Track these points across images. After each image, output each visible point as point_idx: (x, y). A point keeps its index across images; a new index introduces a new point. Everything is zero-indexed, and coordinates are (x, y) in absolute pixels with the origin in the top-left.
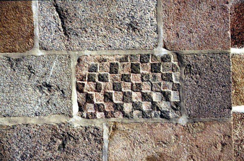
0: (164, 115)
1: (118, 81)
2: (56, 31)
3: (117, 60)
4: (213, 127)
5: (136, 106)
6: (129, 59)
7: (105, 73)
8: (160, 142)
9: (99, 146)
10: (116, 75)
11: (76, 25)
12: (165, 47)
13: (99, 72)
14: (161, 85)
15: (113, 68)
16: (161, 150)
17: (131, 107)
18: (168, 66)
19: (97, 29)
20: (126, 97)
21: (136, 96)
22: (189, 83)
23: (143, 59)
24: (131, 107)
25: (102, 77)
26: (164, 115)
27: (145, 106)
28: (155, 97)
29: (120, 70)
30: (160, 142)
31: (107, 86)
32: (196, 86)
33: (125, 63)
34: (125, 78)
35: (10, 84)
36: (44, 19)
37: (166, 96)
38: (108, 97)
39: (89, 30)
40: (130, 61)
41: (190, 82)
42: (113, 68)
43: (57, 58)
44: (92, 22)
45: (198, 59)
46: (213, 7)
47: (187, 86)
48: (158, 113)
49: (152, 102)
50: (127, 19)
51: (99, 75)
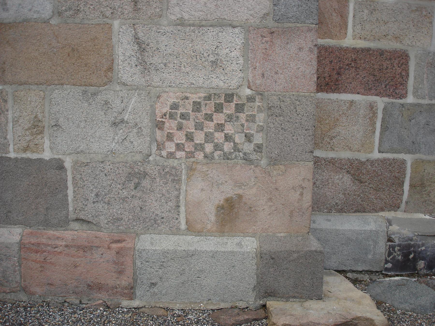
0: (247, 159)
1: (199, 120)
2: (136, 65)
3: (200, 98)
4: (294, 170)
5: (217, 147)
6: (213, 97)
7: (186, 111)
8: (239, 184)
9: (177, 186)
10: (198, 114)
11: (156, 60)
12: (249, 87)
13: (181, 110)
14: (244, 126)
15: (197, 106)
16: (240, 192)
17: (212, 147)
18: (251, 107)
19: (180, 65)
20: (209, 137)
21: (219, 137)
22: (272, 126)
23: (229, 97)
24: (212, 148)
25: (183, 115)
26: (247, 159)
27: (228, 147)
28: (239, 138)
29: (203, 108)
30: (239, 184)
31: (190, 126)
32: (280, 129)
33: (207, 101)
34: (209, 118)
35: (86, 119)
36: (124, 52)
37: (249, 138)
38: (189, 137)
39: (171, 65)
40: (213, 100)
41: (273, 124)
42: (197, 106)
43: (137, 94)
44: (175, 57)
45: (283, 101)
46: (300, 49)
47: (270, 128)
48: (239, 155)
49: (234, 143)
50: (211, 56)
51: (181, 113)
